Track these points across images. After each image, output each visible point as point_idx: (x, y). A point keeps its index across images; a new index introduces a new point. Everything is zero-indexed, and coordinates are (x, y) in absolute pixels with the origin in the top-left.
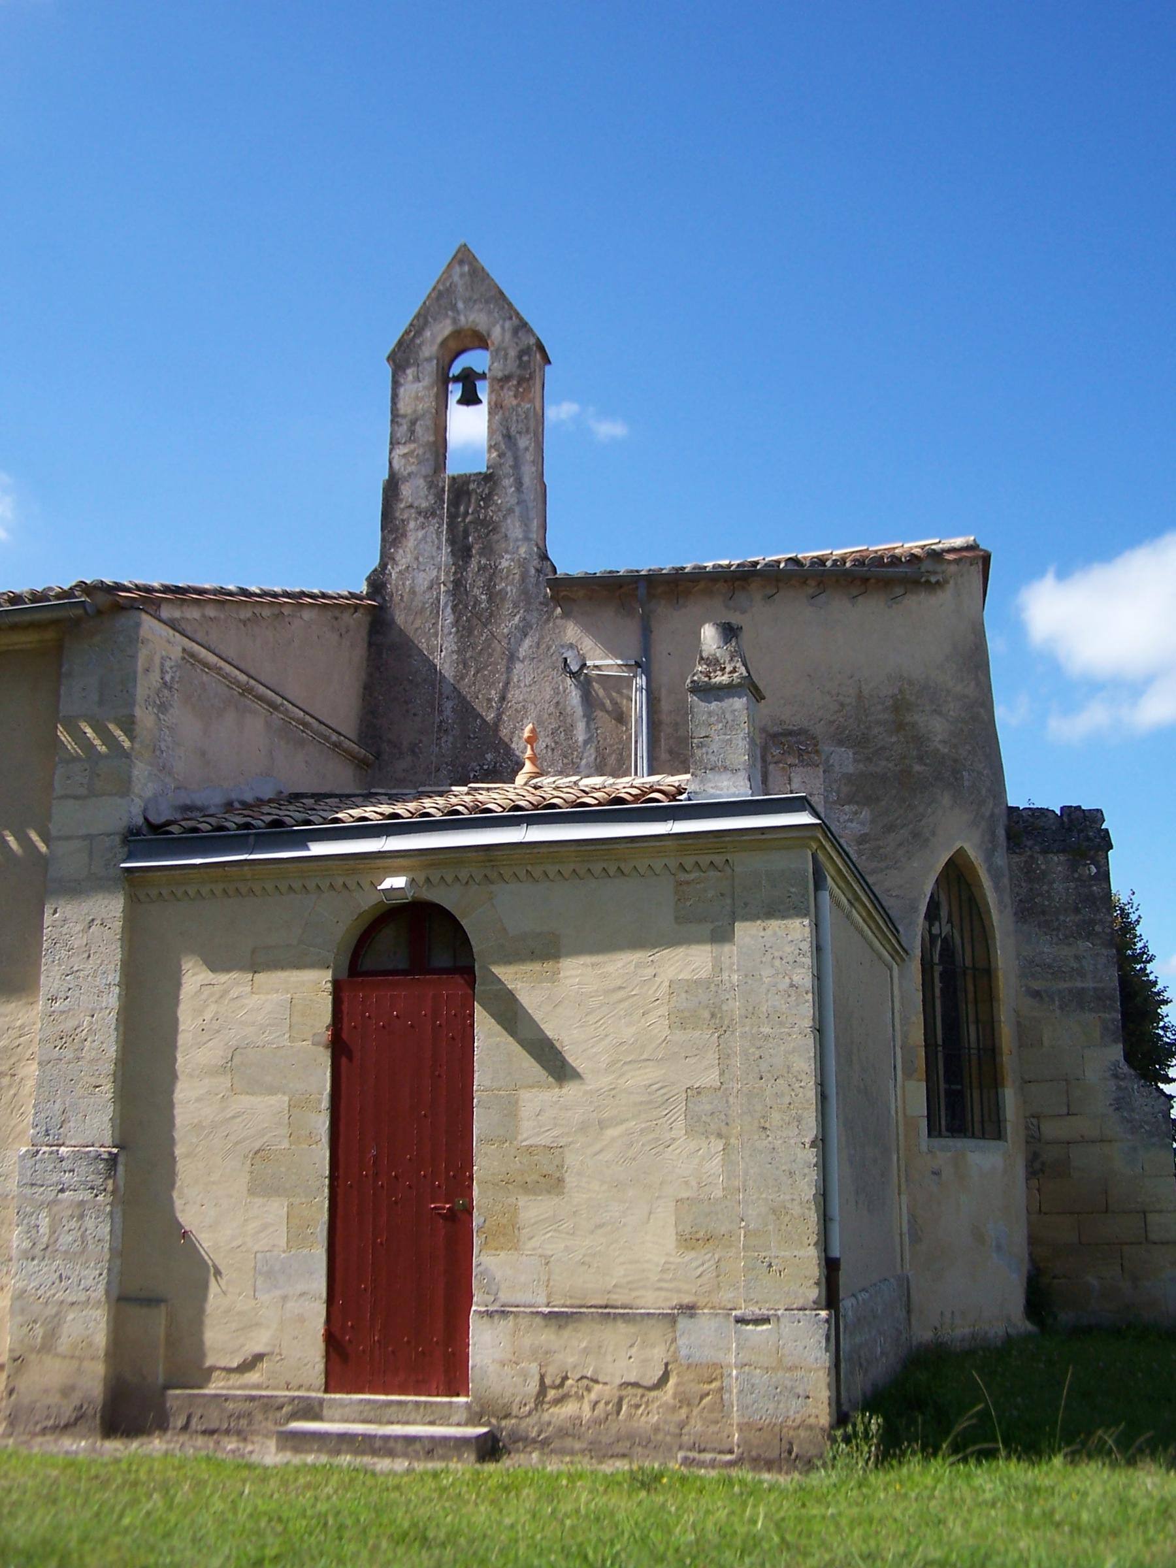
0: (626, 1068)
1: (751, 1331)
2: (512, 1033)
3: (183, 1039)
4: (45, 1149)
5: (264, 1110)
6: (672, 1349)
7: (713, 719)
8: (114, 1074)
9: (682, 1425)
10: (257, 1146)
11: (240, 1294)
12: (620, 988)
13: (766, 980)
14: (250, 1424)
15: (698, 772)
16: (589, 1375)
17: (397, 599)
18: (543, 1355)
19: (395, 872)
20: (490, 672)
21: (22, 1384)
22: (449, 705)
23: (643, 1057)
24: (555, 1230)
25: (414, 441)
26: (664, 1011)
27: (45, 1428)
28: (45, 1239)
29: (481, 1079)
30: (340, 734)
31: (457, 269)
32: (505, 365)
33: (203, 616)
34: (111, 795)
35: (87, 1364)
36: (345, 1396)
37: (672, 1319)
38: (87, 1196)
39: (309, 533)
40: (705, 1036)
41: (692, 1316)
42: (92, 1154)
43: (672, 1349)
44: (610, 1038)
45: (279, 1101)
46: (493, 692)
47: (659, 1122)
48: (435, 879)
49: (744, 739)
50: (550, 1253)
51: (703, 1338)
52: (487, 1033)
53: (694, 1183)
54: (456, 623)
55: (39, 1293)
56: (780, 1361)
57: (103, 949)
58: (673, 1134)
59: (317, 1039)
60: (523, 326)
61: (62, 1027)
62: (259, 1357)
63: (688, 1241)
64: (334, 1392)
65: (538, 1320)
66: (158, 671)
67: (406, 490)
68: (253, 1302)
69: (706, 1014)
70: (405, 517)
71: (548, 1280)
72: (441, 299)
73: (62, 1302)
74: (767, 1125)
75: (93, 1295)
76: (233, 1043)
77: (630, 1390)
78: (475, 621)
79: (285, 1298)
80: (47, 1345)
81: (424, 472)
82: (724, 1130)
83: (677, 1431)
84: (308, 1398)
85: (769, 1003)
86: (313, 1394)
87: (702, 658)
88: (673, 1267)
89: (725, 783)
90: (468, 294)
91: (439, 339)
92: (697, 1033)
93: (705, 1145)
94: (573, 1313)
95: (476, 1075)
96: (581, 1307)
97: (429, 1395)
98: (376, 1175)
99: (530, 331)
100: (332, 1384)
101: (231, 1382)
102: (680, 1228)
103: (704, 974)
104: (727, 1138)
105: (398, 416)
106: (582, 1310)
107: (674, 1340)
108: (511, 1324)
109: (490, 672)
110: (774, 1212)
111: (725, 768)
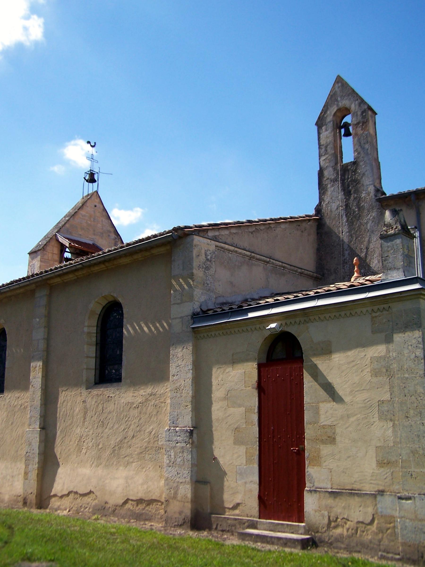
0: (356, 393)
1: (404, 503)
2: (316, 381)
3: (214, 388)
4: (172, 428)
5: (238, 412)
6: (375, 509)
7: (389, 249)
8: (192, 402)
9: (380, 541)
10: (236, 426)
11: (232, 481)
12: (353, 361)
13: (406, 355)
14: (235, 529)
15: (385, 271)
16: (346, 517)
17: (326, 214)
18: (329, 508)
19: (273, 322)
20: (361, 238)
21: (168, 510)
22: (347, 253)
23: (362, 389)
24: (333, 459)
25: (327, 154)
26: (369, 370)
27: (175, 525)
28: (173, 460)
29: (306, 399)
30: (301, 269)
31: (337, 86)
32: (357, 119)
33: (230, 233)
34: (187, 302)
35: (186, 504)
36: (265, 520)
37: (374, 496)
38: (184, 445)
39: (293, 194)
40: (384, 379)
41: (382, 495)
42: (185, 430)
43: (375, 509)
44: (350, 381)
45: (242, 409)
46: (362, 246)
47: (369, 414)
48: (288, 323)
49: (401, 255)
50: (331, 467)
51: (387, 504)
52: (308, 382)
53: (382, 440)
54: (347, 221)
55: (172, 478)
56: (416, 517)
57: (187, 357)
58: (375, 420)
59: (253, 386)
60: (363, 101)
61: (176, 385)
62: (238, 505)
63: (381, 464)
64: (262, 519)
65: (327, 494)
66: (204, 255)
67: (326, 173)
68: (236, 484)
69: (384, 370)
70: (327, 183)
71: (331, 479)
72: (332, 98)
73: (178, 482)
74: (408, 416)
75: (187, 480)
76: (228, 389)
77: (361, 525)
78: (354, 219)
79: (246, 483)
80: (175, 497)
81: (332, 165)
82: (393, 418)
83: (378, 543)
84: (253, 520)
85: (408, 364)
86: (255, 519)
87: (385, 225)
88: (375, 474)
89: (395, 275)
90: (341, 94)
91: (333, 114)
92: (381, 378)
93: (386, 425)
94: (339, 492)
95: (305, 398)
96: (343, 489)
97: (293, 522)
98: (274, 437)
99: (365, 103)
100: (261, 516)
101: (230, 513)
102: (378, 459)
103: (383, 354)
104: (394, 421)
105: (321, 145)
106: (342, 491)
107: (376, 505)
108: (318, 495)
109: (361, 238)
110: (412, 452)
111: (395, 268)
